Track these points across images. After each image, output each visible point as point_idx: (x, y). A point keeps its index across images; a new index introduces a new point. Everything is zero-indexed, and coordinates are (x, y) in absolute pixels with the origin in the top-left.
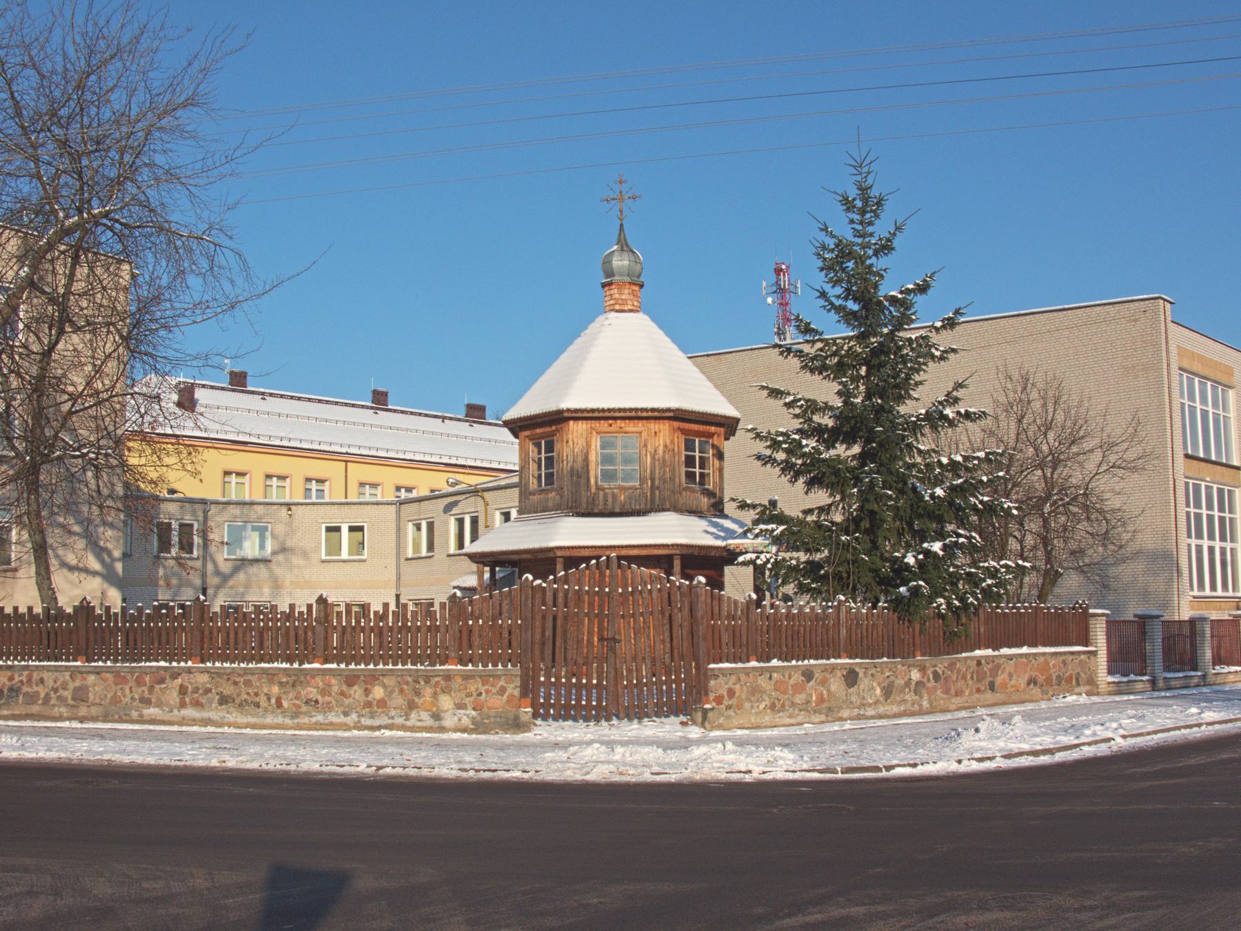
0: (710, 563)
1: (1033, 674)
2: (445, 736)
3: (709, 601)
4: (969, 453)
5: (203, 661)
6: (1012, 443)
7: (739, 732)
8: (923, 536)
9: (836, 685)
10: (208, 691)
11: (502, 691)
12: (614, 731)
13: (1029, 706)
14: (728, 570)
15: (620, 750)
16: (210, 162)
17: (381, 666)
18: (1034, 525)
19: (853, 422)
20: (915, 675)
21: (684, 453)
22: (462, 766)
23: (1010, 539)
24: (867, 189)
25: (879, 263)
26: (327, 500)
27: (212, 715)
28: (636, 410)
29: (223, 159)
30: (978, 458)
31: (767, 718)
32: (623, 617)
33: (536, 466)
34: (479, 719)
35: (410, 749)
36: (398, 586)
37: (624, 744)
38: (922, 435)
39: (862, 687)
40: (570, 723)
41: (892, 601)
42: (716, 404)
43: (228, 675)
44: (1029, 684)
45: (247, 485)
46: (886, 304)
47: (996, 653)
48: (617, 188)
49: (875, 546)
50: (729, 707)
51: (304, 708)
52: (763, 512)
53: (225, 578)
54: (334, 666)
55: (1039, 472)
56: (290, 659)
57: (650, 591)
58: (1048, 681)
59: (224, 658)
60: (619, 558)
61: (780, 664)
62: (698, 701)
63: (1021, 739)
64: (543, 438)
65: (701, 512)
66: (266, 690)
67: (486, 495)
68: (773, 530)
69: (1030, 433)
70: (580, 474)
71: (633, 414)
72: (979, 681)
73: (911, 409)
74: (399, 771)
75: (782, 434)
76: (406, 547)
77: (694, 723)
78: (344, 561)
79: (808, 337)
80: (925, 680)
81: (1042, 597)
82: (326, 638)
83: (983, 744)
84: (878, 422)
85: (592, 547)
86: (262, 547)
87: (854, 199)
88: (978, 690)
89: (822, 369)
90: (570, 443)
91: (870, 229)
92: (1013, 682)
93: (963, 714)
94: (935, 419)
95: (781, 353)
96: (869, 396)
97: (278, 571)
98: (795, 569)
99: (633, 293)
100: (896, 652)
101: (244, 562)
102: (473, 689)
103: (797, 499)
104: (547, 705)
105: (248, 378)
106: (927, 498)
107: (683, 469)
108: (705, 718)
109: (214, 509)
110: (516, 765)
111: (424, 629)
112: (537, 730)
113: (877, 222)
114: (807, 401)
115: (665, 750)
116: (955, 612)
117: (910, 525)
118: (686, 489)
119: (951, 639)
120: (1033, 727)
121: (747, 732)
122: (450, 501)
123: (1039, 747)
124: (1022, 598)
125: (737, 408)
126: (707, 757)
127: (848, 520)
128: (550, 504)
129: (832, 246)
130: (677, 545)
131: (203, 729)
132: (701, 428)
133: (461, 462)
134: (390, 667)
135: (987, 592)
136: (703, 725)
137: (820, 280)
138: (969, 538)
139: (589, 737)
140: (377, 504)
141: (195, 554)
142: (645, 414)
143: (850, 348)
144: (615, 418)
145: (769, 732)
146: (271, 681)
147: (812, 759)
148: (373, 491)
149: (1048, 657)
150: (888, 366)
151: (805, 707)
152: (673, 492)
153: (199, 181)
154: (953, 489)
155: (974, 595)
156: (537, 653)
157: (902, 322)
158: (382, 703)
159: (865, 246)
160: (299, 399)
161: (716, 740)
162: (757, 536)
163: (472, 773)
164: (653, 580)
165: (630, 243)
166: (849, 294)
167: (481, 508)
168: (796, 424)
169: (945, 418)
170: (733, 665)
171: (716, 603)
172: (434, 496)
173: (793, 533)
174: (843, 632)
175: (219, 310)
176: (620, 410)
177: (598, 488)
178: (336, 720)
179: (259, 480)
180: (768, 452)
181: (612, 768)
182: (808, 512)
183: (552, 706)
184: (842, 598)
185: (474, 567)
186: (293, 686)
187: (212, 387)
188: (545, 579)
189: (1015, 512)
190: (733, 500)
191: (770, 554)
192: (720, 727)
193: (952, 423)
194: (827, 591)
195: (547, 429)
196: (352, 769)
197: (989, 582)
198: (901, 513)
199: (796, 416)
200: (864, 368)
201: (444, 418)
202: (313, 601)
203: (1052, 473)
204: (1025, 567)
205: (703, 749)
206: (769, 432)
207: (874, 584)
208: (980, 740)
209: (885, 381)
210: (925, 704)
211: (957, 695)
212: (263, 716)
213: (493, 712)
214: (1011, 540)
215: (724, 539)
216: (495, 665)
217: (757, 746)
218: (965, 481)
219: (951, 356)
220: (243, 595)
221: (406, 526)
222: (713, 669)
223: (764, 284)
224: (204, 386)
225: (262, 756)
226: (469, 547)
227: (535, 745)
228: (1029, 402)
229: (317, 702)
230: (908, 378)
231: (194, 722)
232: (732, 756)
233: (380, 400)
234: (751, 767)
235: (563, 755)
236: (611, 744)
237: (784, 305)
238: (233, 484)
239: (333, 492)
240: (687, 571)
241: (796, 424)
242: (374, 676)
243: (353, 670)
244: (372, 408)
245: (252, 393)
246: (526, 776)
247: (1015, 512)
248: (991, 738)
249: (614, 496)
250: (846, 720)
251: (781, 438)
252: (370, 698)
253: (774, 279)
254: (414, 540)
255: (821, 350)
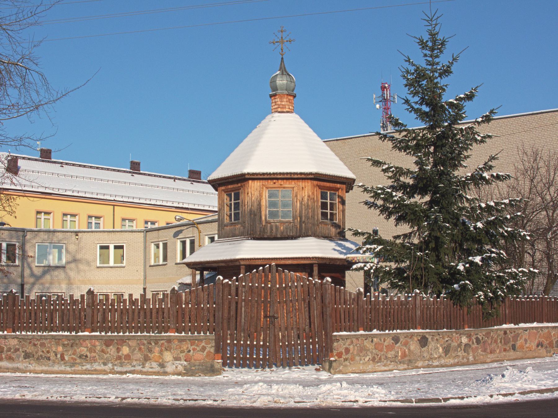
0: (336, 269)
1: (541, 340)
2: (167, 378)
3: (333, 293)
4: (500, 201)
5: (14, 331)
6: (527, 194)
7: (352, 375)
8: (469, 253)
9: (414, 346)
10: (17, 350)
11: (204, 349)
12: (274, 374)
13: (538, 360)
14: (348, 273)
15: (275, 387)
16: (20, 16)
17: (127, 334)
18: (541, 246)
19: (425, 181)
20: (464, 340)
21: (320, 200)
22: (175, 397)
23: (526, 254)
24: (435, 35)
25: (442, 82)
26: (101, 229)
27: (19, 365)
28: (291, 174)
29: (30, 15)
30: (504, 204)
31: (370, 366)
32: (279, 302)
33: (228, 208)
34: (189, 367)
35: (144, 386)
36: (145, 283)
37: (277, 383)
38: (469, 189)
39: (430, 347)
40: (246, 369)
41: (449, 293)
42: (342, 170)
43: (30, 340)
44: (538, 346)
45: (51, 220)
46: (447, 107)
47: (517, 326)
48: (280, 35)
49: (439, 259)
50: (346, 360)
51: (78, 361)
52: (369, 238)
53: (38, 278)
54: (98, 334)
55: (544, 213)
56: (70, 330)
57: (296, 287)
58: (551, 344)
59: (27, 329)
60: (277, 266)
61: (378, 332)
62: (327, 355)
63: (532, 382)
64: (233, 191)
65: (331, 237)
66: (54, 349)
67: (199, 226)
68: (375, 249)
69: (539, 188)
70: (256, 214)
71: (289, 176)
72: (505, 344)
73: (461, 173)
74: (136, 400)
75: (380, 189)
76: (150, 258)
77: (324, 369)
78: (111, 267)
79: (397, 128)
80: (471, 343)
81: (546, 291)
82: (93, 316)
83: (507, 385)
84: (440, 181)
85: (263, 259)
86: (60, 258)
87: (427, 41)
88: (505, 350)
89: (406, 148)
90: (250, 194)
91: (437, 60)
92: (527, 345)
93: (495, 365)
94: (477, 179)
95: (381, 138)
96: (435, 165)
97: (72, 274)
98: (388, 273)
99: (289, 101)
100: (410, 325)
101: (49, 269)
102: (185, 348)
103: (391, 229)
104: (232, 358)
105: (52, 154)
106: (472, 229)
107: (320, 211)
108: (330, 366)
109: (29, 236)
110: (210, 396)
111: (113, 310)
112: (225, 374)
113: (441, 55)
114: (396, 168)
115: (304, 387)
116: (490, 300)
117: (461, 245)
118: (321, 223)
119: (488, 316)
120: (540, 375)
121: (357, 375)
122: (177, 229)
123: (543, 388)
124: (533, 291)
125: (354, 173)
126: (330, 392)
127: (421, 242)
128: (237, 232)
129: (413, 71)
130: (316, 258)
131: (13, 375)
132: (331, 185)
133: (185, 206)
134: (133, 334)
135: (510, 289)
136: (329, 371)
137: (405, 92)
138: (499, 254)
139: (258, 378)
140: (132, 232)
141: (17, 263)
142: (296, 176)
143: (424, 135)
144: (278, 179)
145: (371, 376)
146: (58, 344)
147: (397, 393)
148: (131, 224)
149: (550, 329)
150: (447, 146)
151: (394, 360)
152: (313, 224)
153: (15, 28)
154: (488, 223)
155: (502, 289)
156: (225, 325)
157: (456, 119)
158: (128, 357)
159: (433, 71)
160: (85, 166)
161: (336, 381)
162: (364, 252)
163: (181, 402)
164: (299, 279)
165: (287, 70)
166: (423, 101)
167: (196, 234)
168: (390, 182)
169: (484, 178)
170: (348, 333)
171: (337, 294)
172: (168, 227)
173: (387, 250)
174: (418, 312)
175: (28, 110)
176: (280, 174)
177: (267, 222)
178: (98, 368)
179: (59, 217)
180: (372, 200)
181: (270, 398)
182: (398, 237)
183: (235, 358)
184: (418, 291)
185: (189, 271)
186: (72, 346)
187: (29, 159)
188: (230, 278)
189: (528, 238)
190: (350, 230)
191: (373, 263)
192: (340, 372)
193: (488, 182)
194: (409, 287)
195: (236, 186)
196: (106, 400)
197: (512, 281)
198: (455, 238)
199: (390, 178)
200: (432, 148)
201: (175, 179)
202: (84, 292)
203: (553, 214)
204: (535, 272)
205: (328, 386)
206: (372, 188)
207: (438, 283)
208: (505, 382)
209: (445, 155)
210: (471, 358)
211: (491, 353)
212: (52, 366)
213: (197, 363)
214: (526, 255)
215: (346, 254)
216: (199, 333)
217: (362, 384)
218: (496, 218)
219: (487, 140)
220: (48, 288)
221: (150, 245)
222: (336, 336)
223: (374, 96)
224: (24, 158)
225: (49, 391)
226: (190, 258)
227: (223, 384)
228: (538, 169)
229: (86, 356)
230: (460, 153)
231: (7, 370)
232: (346, 391)
233: (135, 168)
234: (357, 398)
235: (239, 390)
236: (270, 383)
237: (386, 109)
238: (93, 224)
239: (106, 224)
240: (322, 274)
241: (390, 182)
242: (123, 340)
243: (110, 336)
244: (130, 172)
245: (55, 162)
246: (216, 403)
247: (528, 238)
248: (513, 381)
249: (277, 227)
250: (420, 368)
251: (380, 191)
252: (120, 354)
253: (380, 93)
254: (155, 254)
255: (405, 136)
